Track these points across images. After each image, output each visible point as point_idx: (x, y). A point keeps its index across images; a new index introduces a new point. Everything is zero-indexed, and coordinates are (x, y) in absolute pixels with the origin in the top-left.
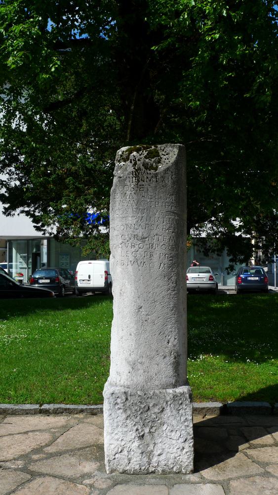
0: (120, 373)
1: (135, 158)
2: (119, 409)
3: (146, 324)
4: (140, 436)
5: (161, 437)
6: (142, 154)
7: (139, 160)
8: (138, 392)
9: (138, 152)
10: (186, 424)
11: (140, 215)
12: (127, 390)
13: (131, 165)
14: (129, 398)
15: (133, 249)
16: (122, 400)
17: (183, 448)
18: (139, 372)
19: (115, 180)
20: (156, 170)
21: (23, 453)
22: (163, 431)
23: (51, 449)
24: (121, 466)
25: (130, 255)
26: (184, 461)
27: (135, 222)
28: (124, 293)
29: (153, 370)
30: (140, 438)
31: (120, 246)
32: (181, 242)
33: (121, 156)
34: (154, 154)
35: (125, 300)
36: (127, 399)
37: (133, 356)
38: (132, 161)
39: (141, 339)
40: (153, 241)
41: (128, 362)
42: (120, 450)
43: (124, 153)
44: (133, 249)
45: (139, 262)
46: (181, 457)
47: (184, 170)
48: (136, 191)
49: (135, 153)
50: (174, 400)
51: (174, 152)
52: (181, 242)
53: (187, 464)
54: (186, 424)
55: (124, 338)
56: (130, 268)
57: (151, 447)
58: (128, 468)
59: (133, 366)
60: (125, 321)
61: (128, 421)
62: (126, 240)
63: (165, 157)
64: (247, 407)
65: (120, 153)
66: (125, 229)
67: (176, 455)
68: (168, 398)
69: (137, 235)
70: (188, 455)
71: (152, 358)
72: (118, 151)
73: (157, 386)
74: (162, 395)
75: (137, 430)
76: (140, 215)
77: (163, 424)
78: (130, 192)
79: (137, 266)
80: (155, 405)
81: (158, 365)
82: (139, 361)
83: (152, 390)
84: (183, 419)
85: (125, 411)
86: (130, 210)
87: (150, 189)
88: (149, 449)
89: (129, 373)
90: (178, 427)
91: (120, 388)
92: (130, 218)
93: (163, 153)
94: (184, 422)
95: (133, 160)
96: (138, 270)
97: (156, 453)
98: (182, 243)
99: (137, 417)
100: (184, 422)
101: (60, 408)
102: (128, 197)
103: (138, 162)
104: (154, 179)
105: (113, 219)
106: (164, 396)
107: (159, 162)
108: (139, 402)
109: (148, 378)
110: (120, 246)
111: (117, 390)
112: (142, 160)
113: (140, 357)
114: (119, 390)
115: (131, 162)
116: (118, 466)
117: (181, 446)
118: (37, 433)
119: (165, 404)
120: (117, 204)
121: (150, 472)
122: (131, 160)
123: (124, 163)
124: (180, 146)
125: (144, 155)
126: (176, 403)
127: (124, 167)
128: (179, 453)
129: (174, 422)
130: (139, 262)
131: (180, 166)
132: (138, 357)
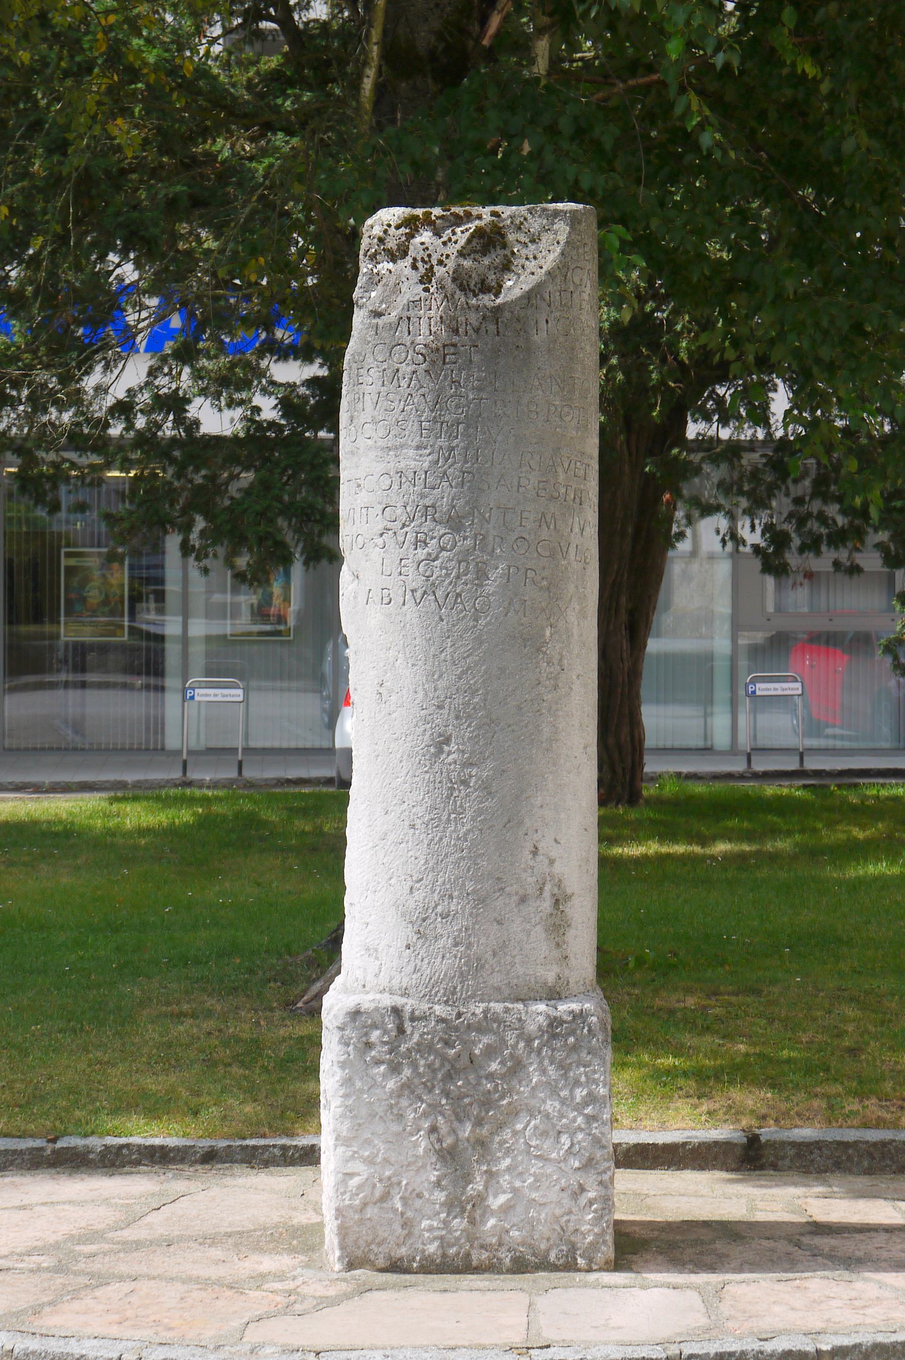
0: (376, 957)
1: (429, 256)
2: (378, 1062)
3: (463, 794)
4: (441, 1150)
5: (508, 1152)
6: (450, 240)
7: (440, 263)
8: (437, 1007)
9: (438, 234)
10: (588, 1110)
11: (442, 442)
12: (399, 1001)
13: (415, 276)
14: (408, 1026)
15: (422, 553)
16: (386, 1032)
17: (582, 1189)
18: (441, 943)
19: (359, 318)
20: (497, 295)
21: (39, 1244)
22: (515, 1133)
23: (129, 1234)
24: (379, 1245)
25: (411, 570)
26: (585, 1228)
27: (426, 465)
28: (390, 691)
29: (483, 941)
30: (443, 1157)
31: (380, 541)
32: (576, 529)
33: (381, 240)
34: (489, 240)
35: (394, 715)
36: (401, 1030)
37: (419, 895)
38: (420, 264)
39: (445, 841)
40: (486, 525)
41: (403, 915)
42: (377, 1194)
43: (392, 231)
44: (422, 553)
45: (440, 593)
46: (573, 1217)
47: (588, 290)
48: (433, 362)
49: (426, 236)
50: (554, 1036)
51: (556, 233)
52: (576, 529)
53: (590, 1238)
54: (588, 1110)
55: (392, 837)
56: (411, 612)
57: (477, 1185)
58: (403, 1251)
59: (422, 928)
60: (394, 785)
61: (404, 1102)
62: (398, 524)
63: (524, 252)
64: (839, 1143)
65: (377, 231)
66: (395, 487)
67: (558, 1212)
68: (532, 1027)
69: (433, 506)
70: (595, 1211)
71: (482, 901)
72: (369, 222)
73: (499, 989)
74: (511, 1019)
75: (433, 1129)
76: (442, 442)
77: (514, 1112)
78: (412, 368)
79: (434, 605)
80: (490, 1052)
81: (500, 923)
82: (439, 909)
83: (482, 1001)
84: (580, 1093)
85: (395, 1069)
86: (412, 426)
87: (476, 358)
88: (470, 1190)
89: (408, 947)
90: (564, 1121)
91: (378, 996)
92: (411, 453)
93: (523, 238)
94: (585, 1103)
95: (423, 260)
96: (437, 618)
97: (497, 1202)
98: (582, 530)
99: (433, 1087)
100: (585, 1103)
101: (127, 1146)
102: (404, 384)
103: (439, 271)
104: (492, 328)
105: (352, 453)
106: (520, 1020)
107: (506, 267)
108: (441, 1039)
109: (466, 964)
110: (380, 541)
111: (367, 1001)
112: (451, 264)
113: (442, 897)
114: (373, 1000)
115: (414, 267)
116: (373, 1246)
117: (574, 1180)
118: (66, 1207)
119: (522, 1045)
120: (368, 402)
121: (475, 1263)
122: (415, 259)
123: (391, 266)
124: (574, 212)
125: (458, 247)
126: (557, 1044)
127: (392, 280)
128: (567, 1202)
129: (551, 1106)
130: (440, 593)
131: (577, 280)
132: (436, 897)
